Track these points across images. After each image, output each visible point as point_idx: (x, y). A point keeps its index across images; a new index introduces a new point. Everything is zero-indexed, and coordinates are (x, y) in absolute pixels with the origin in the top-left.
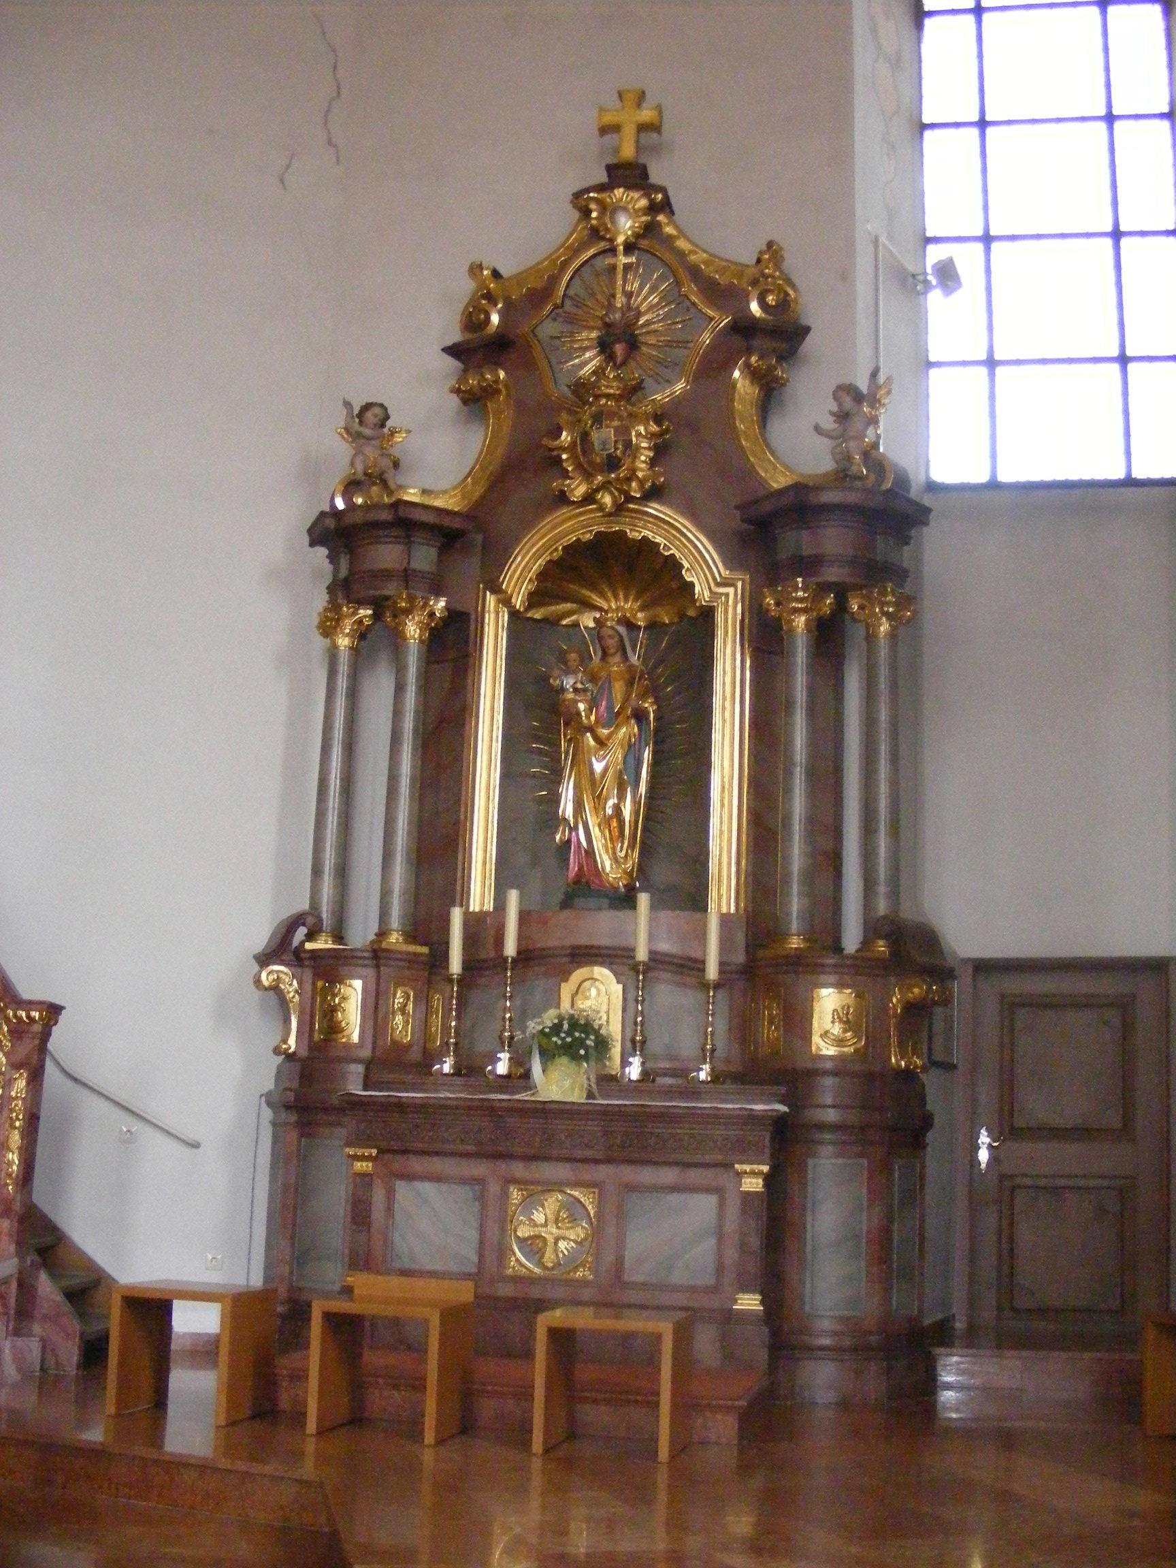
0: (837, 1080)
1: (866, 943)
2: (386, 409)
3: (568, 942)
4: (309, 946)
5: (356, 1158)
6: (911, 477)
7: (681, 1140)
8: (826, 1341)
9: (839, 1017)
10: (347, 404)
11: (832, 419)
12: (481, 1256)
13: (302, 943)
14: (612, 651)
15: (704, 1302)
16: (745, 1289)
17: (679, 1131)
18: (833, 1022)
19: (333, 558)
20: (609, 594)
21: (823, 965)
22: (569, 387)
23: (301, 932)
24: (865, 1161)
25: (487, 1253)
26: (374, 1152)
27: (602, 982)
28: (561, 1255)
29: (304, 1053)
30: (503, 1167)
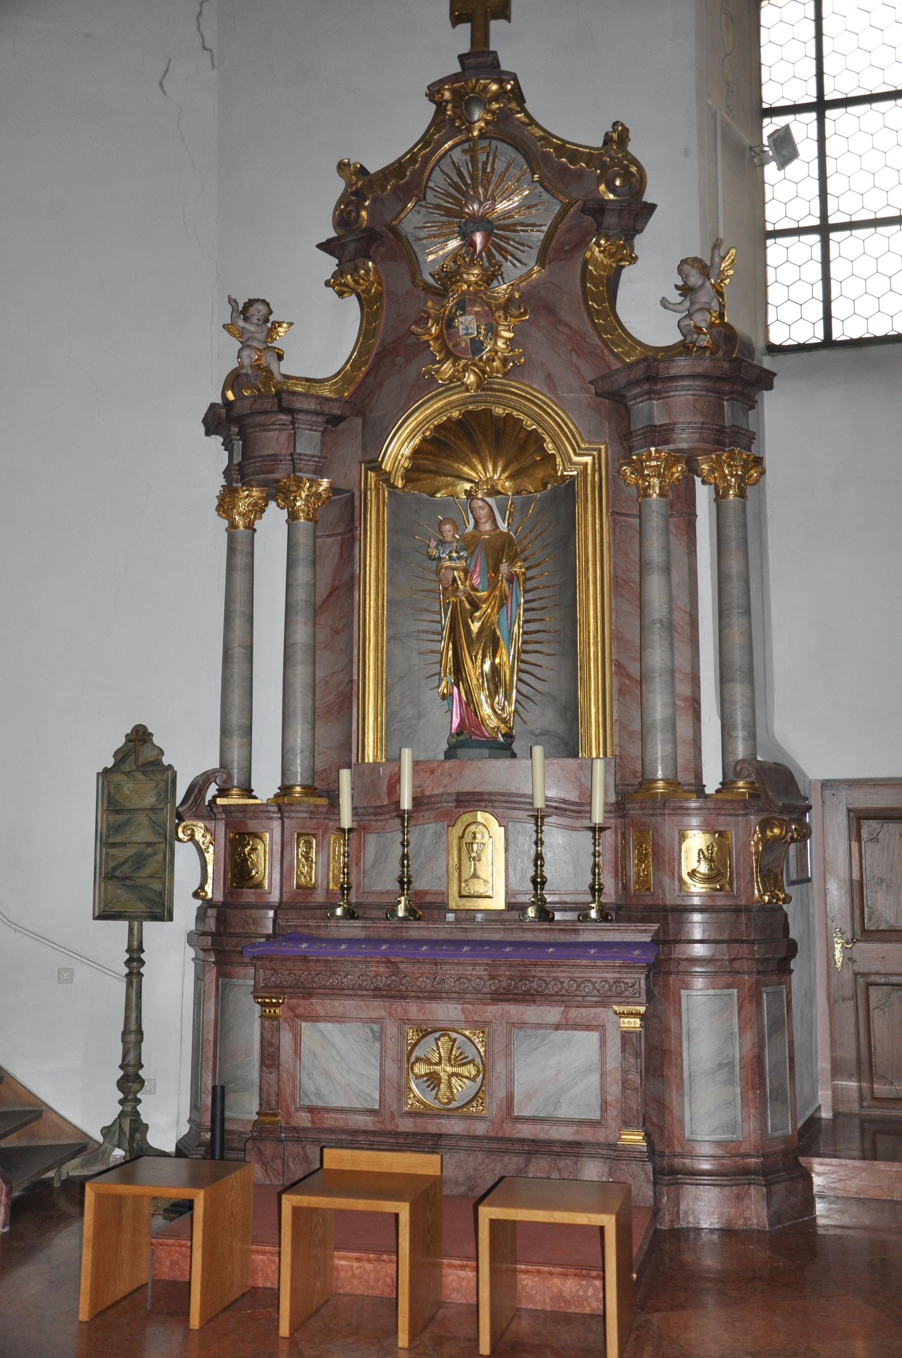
0: (706, 915)
1: (726, 784)
2: (268, 304)
3: (453, 790)
4: (219, 801)
5: (622, 1015)
6: (755, 346)
7: (562, 983)
8: (706, 1166)
9: (704, 857)
10: (232, 301)
11: (461, 27)
12: (382, 1094)
13: (215, 797)
14: (483, 520)
15: (588, 1135)
16: (626, 1124)
17: (559, 974)
18: (699, 861)
19: (228, 446)
20: (499, 469)
21: (687, 809)
22: (433, 276)
23: (212, 790)
24: (735, 991)
25: (387, 1091)
26: (558, 916)
27: (485, 826)
28: (455, 1091)
29: (220, 898)
30: (399, 1007)
